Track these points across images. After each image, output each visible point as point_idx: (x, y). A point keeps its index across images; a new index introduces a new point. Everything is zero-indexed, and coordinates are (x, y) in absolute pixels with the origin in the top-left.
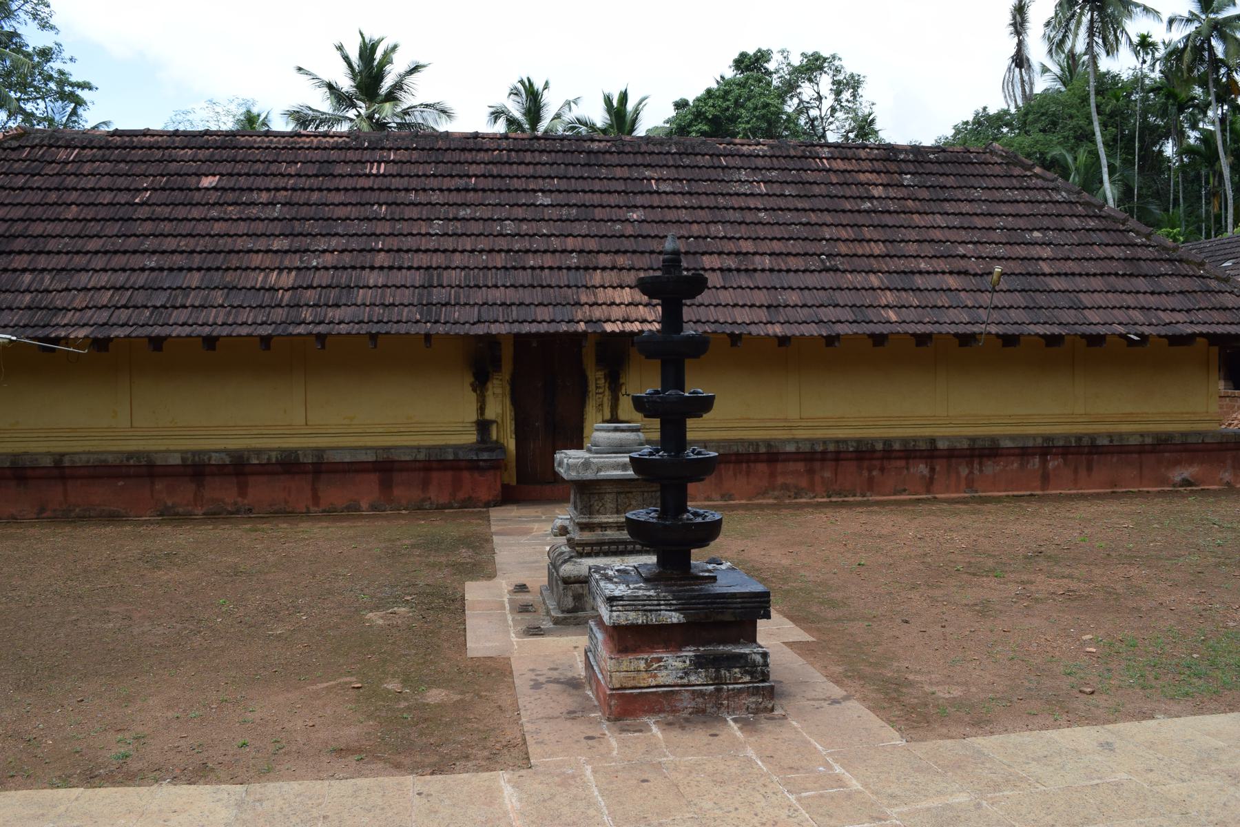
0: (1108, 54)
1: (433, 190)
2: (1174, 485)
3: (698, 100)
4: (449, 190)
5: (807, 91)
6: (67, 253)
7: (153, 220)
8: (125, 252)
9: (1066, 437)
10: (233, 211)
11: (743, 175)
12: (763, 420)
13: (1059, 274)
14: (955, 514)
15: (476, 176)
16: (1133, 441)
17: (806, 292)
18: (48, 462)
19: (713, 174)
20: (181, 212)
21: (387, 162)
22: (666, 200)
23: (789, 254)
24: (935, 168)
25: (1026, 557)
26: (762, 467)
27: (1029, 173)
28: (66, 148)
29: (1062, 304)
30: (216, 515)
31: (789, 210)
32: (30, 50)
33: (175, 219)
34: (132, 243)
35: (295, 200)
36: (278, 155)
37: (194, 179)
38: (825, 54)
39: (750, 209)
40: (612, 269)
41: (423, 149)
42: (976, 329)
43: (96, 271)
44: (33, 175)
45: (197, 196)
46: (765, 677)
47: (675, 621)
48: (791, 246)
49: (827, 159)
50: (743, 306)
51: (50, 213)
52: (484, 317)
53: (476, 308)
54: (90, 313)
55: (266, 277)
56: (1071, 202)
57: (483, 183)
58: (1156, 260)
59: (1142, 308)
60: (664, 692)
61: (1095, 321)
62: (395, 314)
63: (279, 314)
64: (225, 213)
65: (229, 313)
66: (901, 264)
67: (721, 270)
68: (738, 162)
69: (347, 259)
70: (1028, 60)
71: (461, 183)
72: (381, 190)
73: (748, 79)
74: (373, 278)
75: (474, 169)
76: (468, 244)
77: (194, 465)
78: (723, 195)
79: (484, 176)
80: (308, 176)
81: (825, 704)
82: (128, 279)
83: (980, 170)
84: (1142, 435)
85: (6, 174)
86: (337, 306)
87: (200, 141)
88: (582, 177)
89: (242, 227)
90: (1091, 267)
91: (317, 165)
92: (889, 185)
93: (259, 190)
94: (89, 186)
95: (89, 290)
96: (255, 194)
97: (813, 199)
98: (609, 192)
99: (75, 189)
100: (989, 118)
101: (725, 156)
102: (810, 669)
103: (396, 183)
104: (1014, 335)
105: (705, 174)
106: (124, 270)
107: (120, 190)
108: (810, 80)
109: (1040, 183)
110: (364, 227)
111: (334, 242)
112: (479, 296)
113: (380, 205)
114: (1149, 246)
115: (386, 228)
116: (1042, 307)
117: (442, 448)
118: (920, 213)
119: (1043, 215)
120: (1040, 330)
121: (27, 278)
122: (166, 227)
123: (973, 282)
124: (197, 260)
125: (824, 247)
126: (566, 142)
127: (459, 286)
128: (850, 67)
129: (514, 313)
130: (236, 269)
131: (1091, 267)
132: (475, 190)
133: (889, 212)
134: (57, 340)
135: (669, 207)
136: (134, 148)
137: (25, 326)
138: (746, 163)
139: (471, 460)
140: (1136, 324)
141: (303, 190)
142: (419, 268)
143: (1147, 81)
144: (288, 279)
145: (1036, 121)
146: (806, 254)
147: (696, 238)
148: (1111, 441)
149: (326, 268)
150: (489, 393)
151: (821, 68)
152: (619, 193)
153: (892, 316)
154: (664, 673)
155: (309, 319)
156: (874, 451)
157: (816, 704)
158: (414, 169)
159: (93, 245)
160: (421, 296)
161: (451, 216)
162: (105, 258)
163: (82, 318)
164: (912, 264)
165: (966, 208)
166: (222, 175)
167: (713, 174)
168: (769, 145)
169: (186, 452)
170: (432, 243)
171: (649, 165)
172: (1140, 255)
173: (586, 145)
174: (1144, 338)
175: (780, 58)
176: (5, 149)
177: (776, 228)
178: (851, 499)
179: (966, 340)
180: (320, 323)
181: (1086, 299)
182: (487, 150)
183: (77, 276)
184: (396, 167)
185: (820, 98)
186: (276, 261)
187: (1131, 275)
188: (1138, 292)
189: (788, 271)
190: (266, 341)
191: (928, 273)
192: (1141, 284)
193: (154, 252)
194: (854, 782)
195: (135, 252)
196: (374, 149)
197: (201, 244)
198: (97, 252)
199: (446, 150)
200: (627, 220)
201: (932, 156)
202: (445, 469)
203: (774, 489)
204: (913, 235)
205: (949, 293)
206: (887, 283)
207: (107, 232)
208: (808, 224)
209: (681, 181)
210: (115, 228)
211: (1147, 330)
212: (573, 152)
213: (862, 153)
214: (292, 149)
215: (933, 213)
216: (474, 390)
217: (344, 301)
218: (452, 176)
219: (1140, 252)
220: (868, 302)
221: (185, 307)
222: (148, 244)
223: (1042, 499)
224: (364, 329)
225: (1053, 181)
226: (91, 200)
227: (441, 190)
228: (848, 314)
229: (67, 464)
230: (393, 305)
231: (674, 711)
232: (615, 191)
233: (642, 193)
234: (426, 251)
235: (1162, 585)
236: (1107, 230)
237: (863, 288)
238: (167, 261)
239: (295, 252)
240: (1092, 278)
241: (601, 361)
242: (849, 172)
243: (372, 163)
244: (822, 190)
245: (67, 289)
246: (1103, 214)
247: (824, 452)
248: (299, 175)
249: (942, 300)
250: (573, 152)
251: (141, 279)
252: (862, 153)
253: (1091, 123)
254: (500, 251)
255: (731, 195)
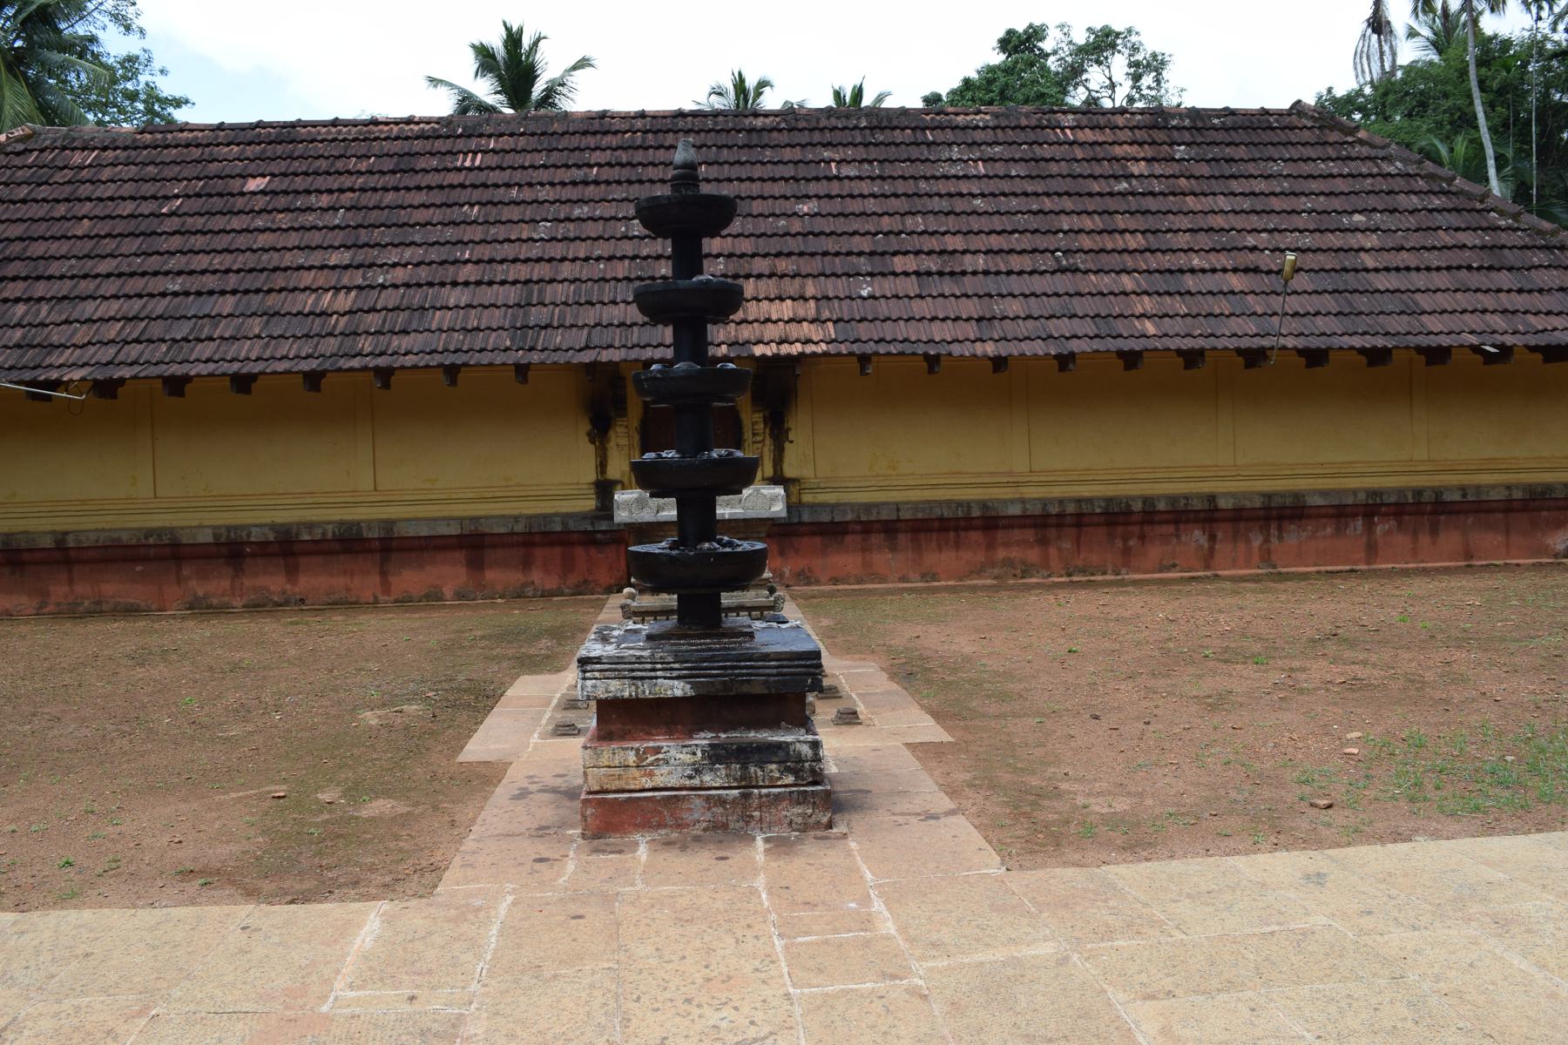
0: (1492, 10)
1: (542, 185)
2: (1556, 556)
3: (953, 92)
4: (563, 184)
5: (1095, 76)
6: (72, 277)
7: (182, 234)
8: (144, 274)
9: (1401, 491)
10: (283, 220)
11: (955, 153)
12: (979, 474)
13: (1387, 269)
14: (1235, 592)
15: (599, 165)
16: (1494, 495)
17: (1033, 299)
18: (47, 542)
19: (914, 152)
20: (219, 223)
21: (485, 152)
22: (847, 187)
23: (1011, 251)
24: (1219, 136)
25: (1313, 641)
26: (976, 536)
27: (1350, 139)
28: (83, 149)
29: (1390, 308)
30: (259, 607)
31: (1015, 195)
32: (111, 61)
33: (210, 231)
34: (153, 263)
35: (363, 202)
36: (346, 149)
37: (239, 181)
38: (1118, 27)
39: (961, 195)
40: (770, 276)
41: (533, 135)
42: (1266, 342)
43: (105, 298)
44: (40, 185)
45: (240, 203)
46: (817, 778)
47: (679, 693)
48: (1015, 241)
49: (1071, 128)
50: (943, 320)
51: (56, 229)
52: (595, 341)
53: (585, 331)
54: (92, 349)
55: (317, 300)
56: (1408, 175)
57: (607, 174)
58: (1526, 247)
59: (1505, 311)
60: (663, 798)
61: (1437, 329)
62: (478, 340)
63: (330, 345)
64: (273, 221)
65: (267, 345)
66: (1166, 261)
67: (917, 274)
68: (949, 136)
69: (423, 274)
70: (1389, 23)
71: (578, 174)
72: (474, 186)
73: (1016, 62)
74: (454, 296)
75: (597, 157)
76: (581, 250)
77: (230, 544)
78: (926, 178)
79: (609, 164)
80: (383, 173)
81: (914, 820)
82: (144, 306)
83: (1282, 136)
84: (1508, 487)
85: (6, 184)
86: (405, 332)
87: (250, 135)
88: (738, 162)
89: (293, 239)
90: (1434, 259)
91: (395, 159)
92: (1154, 159)
93: (320, 192)
94: (107, 195)
95: (95, 321)
96: (313, 198)
97: (1049, 181)
98: (774, 180)
99: (89, 199)
100: (1335, 101)
101: (932, 129)
102: (924, 776)
103: (495, 177)
104: (1318, 350)
105: (904, 152)
106: (140, 296)
107: (144, 198)
108: (1099, 63)
109: (1365, 151)
110: (450, 233)
111: (408, 254)
112: (590, 315)
113: (472, 205)
114: (1518, 229)
115: (477, 233)
116: (1361, 313)
117: (547, 518)
118: (1195, 195)
119: (1368, 193)
120: (1357, 342)
121: (20, 309)
122: (198, 242)
123: (1267, 282)
124: (232, 281)
125: (1061, 240)
126: (720, 118)
127: (565, 304)
128: (1151, 43)
129: (635, 335)
130: (281, 290)
131: (1434, 259)
132: (596, 183)
133: (1153, 194)
134: (55, 385)
135: (852, 196)
136: (167, 147)
137: (10, 368)
138: (960, 137)
139: (585, 532)
140: (1494, 332)
141: (375, 190)
142: (515, 283)
143: (1549, 46)
144: (345, 301)
145: (1399, 102)
146: (1034, 251)
147: (886, 234)
148: (1464, 496)
149: (395, 286)
150: (612, 444)
151: (1113, 46)
152: (787, 180)
153: (1150, 327)
154: (665, 769)
155: (368, 349)
156: (1130, 513)
157: (900, 819)
158: (519, 160)
159: (104, 267)
160: (515, 317)
161: (562, 216)
162: (119, 282)
163: (82, 356)
164: (1182, 260)
165: (1260, 186)
166: (273, 175)
167: (914, 152)
168: (993, 114)
169: (219, 527)
170: (535, 251)
171: (829, 144)
172: (1503, 242)
173: (747, 121)
174: (1505, 351)
175: (1059, 35)
176: (7, 154)
177: (995, 218)
178: (1100, 578)
179: (1252, 357)
180: (380, 355)
181: (1424, 301)
182: (616, 133)
183: (81, 305)
184: (496, 157)
185: (1113, 86)
186: (331, 278)
187: (1490, 268)
188: (1499, 291)
189: (1009, 273)
190: (313, 380)
191: (1203, 271)
192: (1504, 279)
193: (179, 273)
194: (890, 924)
195: (156, 274)
196: (470, 136)
197: (240, 261)
198: (108, 276)
199: (563, 134)
200: (795, 214)
201: (1216, 121)
202: (551, 544)
203: (993, 565)
204: (1185, 222)
205: (1230, 297)
206: (1144, 286)
207: (124, 250)
208: (1040, 211)
209: (871, 162)
210: (132, 245)
211: (1509, 340)
212: (728, 131)
213: (1120, 120)
214: (364, 140)
215: (1214, 194)
216: (592, 441)
217: (414, 326)
218: (568, 167)
219: (1504, 238)
220: (1117, 311)
221: (211, 339)
222: (173, 263)
223: (1363, 575)
224: (436, 359)
225: (1383, 148)
226: (107, 212)
227: (552, 184)
228: (1089, 327)
229: (72, 545)
230: (478, 329)
231: (680, 826)
232: (782, 178)
233: (817, 179)
234: (526, 261)
235: (1495, 670)
236: (1458, 211)
237: (1112, 293)
238: (194, 283)
239: (358, 267)
240: (1434, 274)
241: (758, 400)
242: (1100, 144)
243: (466, 154)
244: (1063, 168)
245: (67, 322)
246: (1453, 189)
247: (1061, 515)
248: (371, 173)
249: (1221, 305)
250: (728, 131)
251: (161, 306)
252: (1120, 120)
253: (1472, 103)
254: (622, 258)
255: (937, 178)
